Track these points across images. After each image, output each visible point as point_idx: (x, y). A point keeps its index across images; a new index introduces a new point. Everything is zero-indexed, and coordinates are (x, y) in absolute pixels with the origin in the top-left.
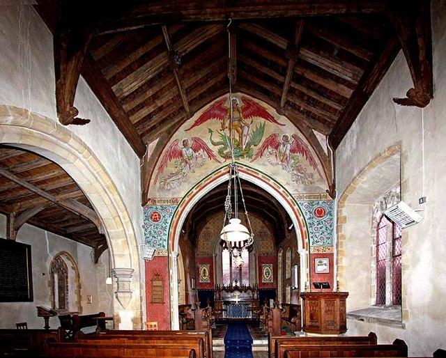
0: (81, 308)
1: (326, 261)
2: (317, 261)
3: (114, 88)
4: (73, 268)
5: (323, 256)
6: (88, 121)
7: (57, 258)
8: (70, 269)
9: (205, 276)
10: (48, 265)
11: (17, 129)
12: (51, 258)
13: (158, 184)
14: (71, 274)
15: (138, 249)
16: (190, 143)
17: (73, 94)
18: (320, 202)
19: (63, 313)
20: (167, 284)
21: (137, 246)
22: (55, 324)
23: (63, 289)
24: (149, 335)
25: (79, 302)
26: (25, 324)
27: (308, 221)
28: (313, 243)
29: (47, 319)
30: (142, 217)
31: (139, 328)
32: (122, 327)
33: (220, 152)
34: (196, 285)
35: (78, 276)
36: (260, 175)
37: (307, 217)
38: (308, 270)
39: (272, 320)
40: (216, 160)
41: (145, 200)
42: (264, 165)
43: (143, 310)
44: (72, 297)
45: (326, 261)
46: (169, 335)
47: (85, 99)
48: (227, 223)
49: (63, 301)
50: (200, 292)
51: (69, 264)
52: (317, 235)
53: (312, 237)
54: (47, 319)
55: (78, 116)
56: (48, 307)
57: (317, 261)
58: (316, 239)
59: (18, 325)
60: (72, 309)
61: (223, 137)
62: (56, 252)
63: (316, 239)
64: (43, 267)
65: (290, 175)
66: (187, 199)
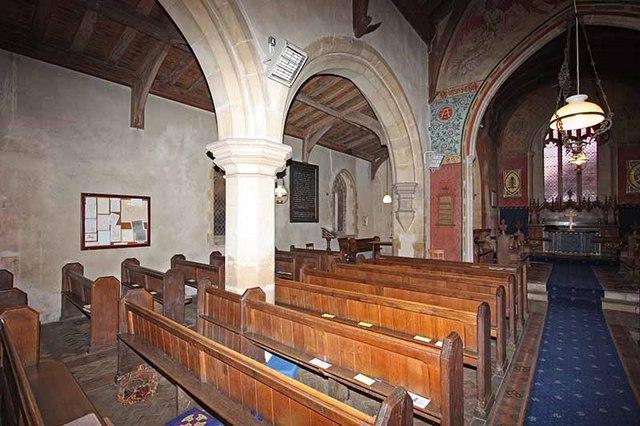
4: (351, 186)
8: (348, 187)
12: (334, 177)
14: (349, 193)
22: (335, 247)
24: (436, 265)
25: (356, 224)
26: (311, 245)
29: (329, 240)
30: (429, 116)
41: (432, 94)
44: (349, 217)
51: (347, 182)
54: (329, 240)
55: (372, 23)
60: (349, 231)
62: (337, 171)
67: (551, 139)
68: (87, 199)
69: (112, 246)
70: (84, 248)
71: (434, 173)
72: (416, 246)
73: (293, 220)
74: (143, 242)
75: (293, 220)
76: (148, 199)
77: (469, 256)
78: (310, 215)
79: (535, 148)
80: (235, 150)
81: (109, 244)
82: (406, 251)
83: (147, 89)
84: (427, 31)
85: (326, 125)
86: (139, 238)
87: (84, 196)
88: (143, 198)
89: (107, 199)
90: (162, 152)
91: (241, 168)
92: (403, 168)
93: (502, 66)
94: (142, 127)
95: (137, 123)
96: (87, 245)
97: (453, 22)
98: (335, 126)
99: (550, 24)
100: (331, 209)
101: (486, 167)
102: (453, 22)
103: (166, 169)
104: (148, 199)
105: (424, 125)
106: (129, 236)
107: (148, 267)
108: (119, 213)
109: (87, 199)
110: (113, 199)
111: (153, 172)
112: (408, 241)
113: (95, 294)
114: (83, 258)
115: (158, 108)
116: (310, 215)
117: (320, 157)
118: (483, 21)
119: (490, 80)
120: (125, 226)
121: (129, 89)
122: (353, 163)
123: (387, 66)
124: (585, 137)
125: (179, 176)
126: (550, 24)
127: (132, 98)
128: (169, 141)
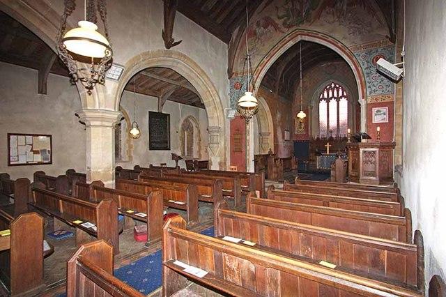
0: (200, 155)
1: (385, 110)
2: (375, 110)
3: (202, 9)
4: (196, 127)
5: (382, 105)
6: (181, 42)
7: (186, 120)
8: (194, 128)
9: (301, 128)
10: (180, 126)
11: (146, 62)
12: (182, 121)
13: (239, 61)
14: (195, 131)
15: (223, 112)
16: (262, 22)
17: (171, 31)
18: (380, 50)
19: (189, 158)
20: (244, 136)
21: (223, 110)
22: (182, 165)
23: (191, 142)
24: (231, 175)
25: (199, 151)
26: (165, 164)
27: (365, 71)
28: (371, 93)
29: (177, 161)
30: (228, 88)
31: (223, 170)
32: (213, 168)
33: (284, 24)
34: (291, 136)
35: (199, 132)
36: (320, 35)
37: (364, 68)
38: (247, 128)
39: (334, 169)
40: (281, 31)
41: (230, 73)
42: (322, 25)
43: (227, 156)
44: (195, 147)
45: (385, 110)
46: (245, 175)
47: (182, 25)
48: (244, 94)
49: (190, 149)
50: (295, 143)
51: (194, 125)
52: (375, 84)
53: (369, 87)
54: (177, 161)
55: (175, 41)
56: (179, 154)
57: (375, 110)
58: (373, 88)
59: (162, 164)
60: (195, 156)
61: (287, 10)
62: (185, 117)
63: (373, 88)
64: (177, 128)
65: (347, 29)
66: (260, 68)
67: (323, 98)
68: (11, 137)
69: (27, 164)
70: (10, 165)
71: (232, 121)
72: (220, 164)
73: (151, 148)
74: (47, 162)
75: (151, 148)
76: (50, 136)
77: (251, 169)
78: (163, 145)
79: (313, 103)
80: (88, 114)
81: (25, 163)
82: (215, 167)
83: (49, 69)
84: (226, 38)
85: (171, 89)
86: (46, 160)
87: (9, 135)
88: (47, 136)
89: (24, 137)
90: (59, 108)
91: (92, 123)
92: (212, 118)
93: (265, 60)
94: (46, 94)
95: (42, 90)
96: (11, 163)
97: (241, 31)
98: (177, 90)
99: (287, 38)
100: (180, 143)
101: (279, 115)
102: (241, 31)
103: (62, 118)
104: (50, 136)
105: (224, 92)
106: (38, 158)
107: (52, 176)
108: (32, 145)
109: (11, 137)
110: (19, 137)
111: (53, 121)
112: (218, 158)
113: (16, 187)
114: (9, 171)
115: (54, 81)
116: (163, 145)
117: (169, 108)
118: (255, 34)
119: (260, 68)
120: (36, 152)
121: (37, 71)
122: (197, 113)
123: (192, 61)
124: (341, 97)
125: (71, 122)
126: (287, 38)
127: (39, 77)
128: (64, 102)
